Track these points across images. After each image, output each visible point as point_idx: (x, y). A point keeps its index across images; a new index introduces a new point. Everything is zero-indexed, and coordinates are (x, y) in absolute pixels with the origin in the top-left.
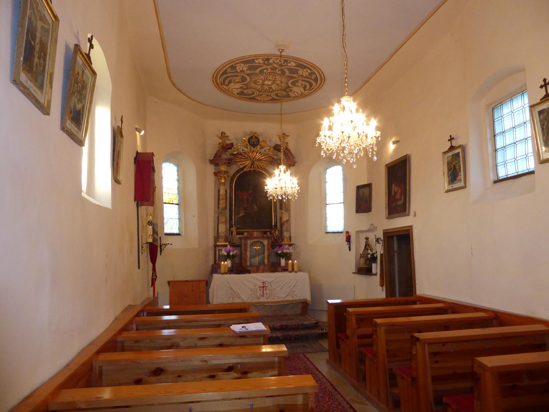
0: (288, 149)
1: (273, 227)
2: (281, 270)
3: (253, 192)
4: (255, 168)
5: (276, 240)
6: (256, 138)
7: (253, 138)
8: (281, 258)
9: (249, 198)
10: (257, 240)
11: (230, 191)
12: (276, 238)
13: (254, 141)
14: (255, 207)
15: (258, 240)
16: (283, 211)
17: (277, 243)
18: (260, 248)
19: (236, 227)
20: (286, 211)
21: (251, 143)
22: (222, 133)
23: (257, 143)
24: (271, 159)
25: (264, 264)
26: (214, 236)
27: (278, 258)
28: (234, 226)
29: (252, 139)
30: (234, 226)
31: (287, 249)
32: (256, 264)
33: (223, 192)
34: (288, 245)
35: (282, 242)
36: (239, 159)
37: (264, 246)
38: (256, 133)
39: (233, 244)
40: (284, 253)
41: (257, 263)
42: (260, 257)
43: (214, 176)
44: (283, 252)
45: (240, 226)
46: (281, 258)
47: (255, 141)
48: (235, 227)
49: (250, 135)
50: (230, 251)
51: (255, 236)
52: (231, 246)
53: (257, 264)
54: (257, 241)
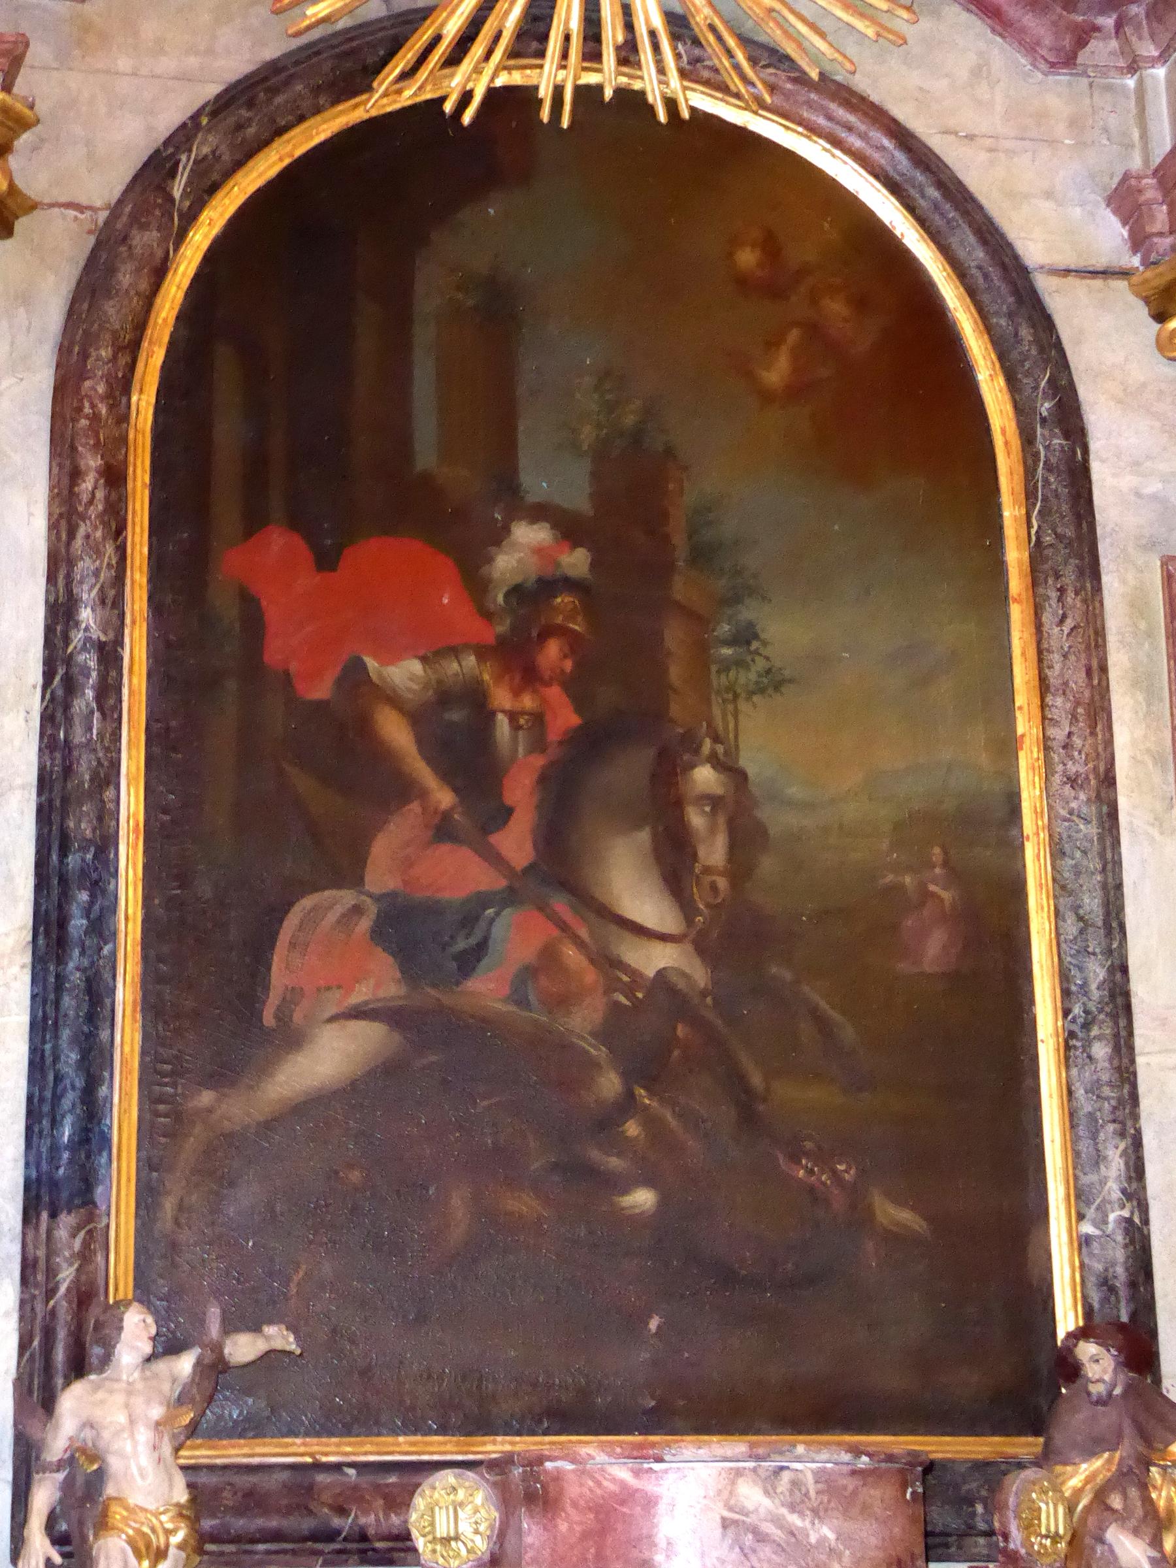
3: (577, 561)
9: (501, 698)
19: (185, 1364)
45: (279, 1337)
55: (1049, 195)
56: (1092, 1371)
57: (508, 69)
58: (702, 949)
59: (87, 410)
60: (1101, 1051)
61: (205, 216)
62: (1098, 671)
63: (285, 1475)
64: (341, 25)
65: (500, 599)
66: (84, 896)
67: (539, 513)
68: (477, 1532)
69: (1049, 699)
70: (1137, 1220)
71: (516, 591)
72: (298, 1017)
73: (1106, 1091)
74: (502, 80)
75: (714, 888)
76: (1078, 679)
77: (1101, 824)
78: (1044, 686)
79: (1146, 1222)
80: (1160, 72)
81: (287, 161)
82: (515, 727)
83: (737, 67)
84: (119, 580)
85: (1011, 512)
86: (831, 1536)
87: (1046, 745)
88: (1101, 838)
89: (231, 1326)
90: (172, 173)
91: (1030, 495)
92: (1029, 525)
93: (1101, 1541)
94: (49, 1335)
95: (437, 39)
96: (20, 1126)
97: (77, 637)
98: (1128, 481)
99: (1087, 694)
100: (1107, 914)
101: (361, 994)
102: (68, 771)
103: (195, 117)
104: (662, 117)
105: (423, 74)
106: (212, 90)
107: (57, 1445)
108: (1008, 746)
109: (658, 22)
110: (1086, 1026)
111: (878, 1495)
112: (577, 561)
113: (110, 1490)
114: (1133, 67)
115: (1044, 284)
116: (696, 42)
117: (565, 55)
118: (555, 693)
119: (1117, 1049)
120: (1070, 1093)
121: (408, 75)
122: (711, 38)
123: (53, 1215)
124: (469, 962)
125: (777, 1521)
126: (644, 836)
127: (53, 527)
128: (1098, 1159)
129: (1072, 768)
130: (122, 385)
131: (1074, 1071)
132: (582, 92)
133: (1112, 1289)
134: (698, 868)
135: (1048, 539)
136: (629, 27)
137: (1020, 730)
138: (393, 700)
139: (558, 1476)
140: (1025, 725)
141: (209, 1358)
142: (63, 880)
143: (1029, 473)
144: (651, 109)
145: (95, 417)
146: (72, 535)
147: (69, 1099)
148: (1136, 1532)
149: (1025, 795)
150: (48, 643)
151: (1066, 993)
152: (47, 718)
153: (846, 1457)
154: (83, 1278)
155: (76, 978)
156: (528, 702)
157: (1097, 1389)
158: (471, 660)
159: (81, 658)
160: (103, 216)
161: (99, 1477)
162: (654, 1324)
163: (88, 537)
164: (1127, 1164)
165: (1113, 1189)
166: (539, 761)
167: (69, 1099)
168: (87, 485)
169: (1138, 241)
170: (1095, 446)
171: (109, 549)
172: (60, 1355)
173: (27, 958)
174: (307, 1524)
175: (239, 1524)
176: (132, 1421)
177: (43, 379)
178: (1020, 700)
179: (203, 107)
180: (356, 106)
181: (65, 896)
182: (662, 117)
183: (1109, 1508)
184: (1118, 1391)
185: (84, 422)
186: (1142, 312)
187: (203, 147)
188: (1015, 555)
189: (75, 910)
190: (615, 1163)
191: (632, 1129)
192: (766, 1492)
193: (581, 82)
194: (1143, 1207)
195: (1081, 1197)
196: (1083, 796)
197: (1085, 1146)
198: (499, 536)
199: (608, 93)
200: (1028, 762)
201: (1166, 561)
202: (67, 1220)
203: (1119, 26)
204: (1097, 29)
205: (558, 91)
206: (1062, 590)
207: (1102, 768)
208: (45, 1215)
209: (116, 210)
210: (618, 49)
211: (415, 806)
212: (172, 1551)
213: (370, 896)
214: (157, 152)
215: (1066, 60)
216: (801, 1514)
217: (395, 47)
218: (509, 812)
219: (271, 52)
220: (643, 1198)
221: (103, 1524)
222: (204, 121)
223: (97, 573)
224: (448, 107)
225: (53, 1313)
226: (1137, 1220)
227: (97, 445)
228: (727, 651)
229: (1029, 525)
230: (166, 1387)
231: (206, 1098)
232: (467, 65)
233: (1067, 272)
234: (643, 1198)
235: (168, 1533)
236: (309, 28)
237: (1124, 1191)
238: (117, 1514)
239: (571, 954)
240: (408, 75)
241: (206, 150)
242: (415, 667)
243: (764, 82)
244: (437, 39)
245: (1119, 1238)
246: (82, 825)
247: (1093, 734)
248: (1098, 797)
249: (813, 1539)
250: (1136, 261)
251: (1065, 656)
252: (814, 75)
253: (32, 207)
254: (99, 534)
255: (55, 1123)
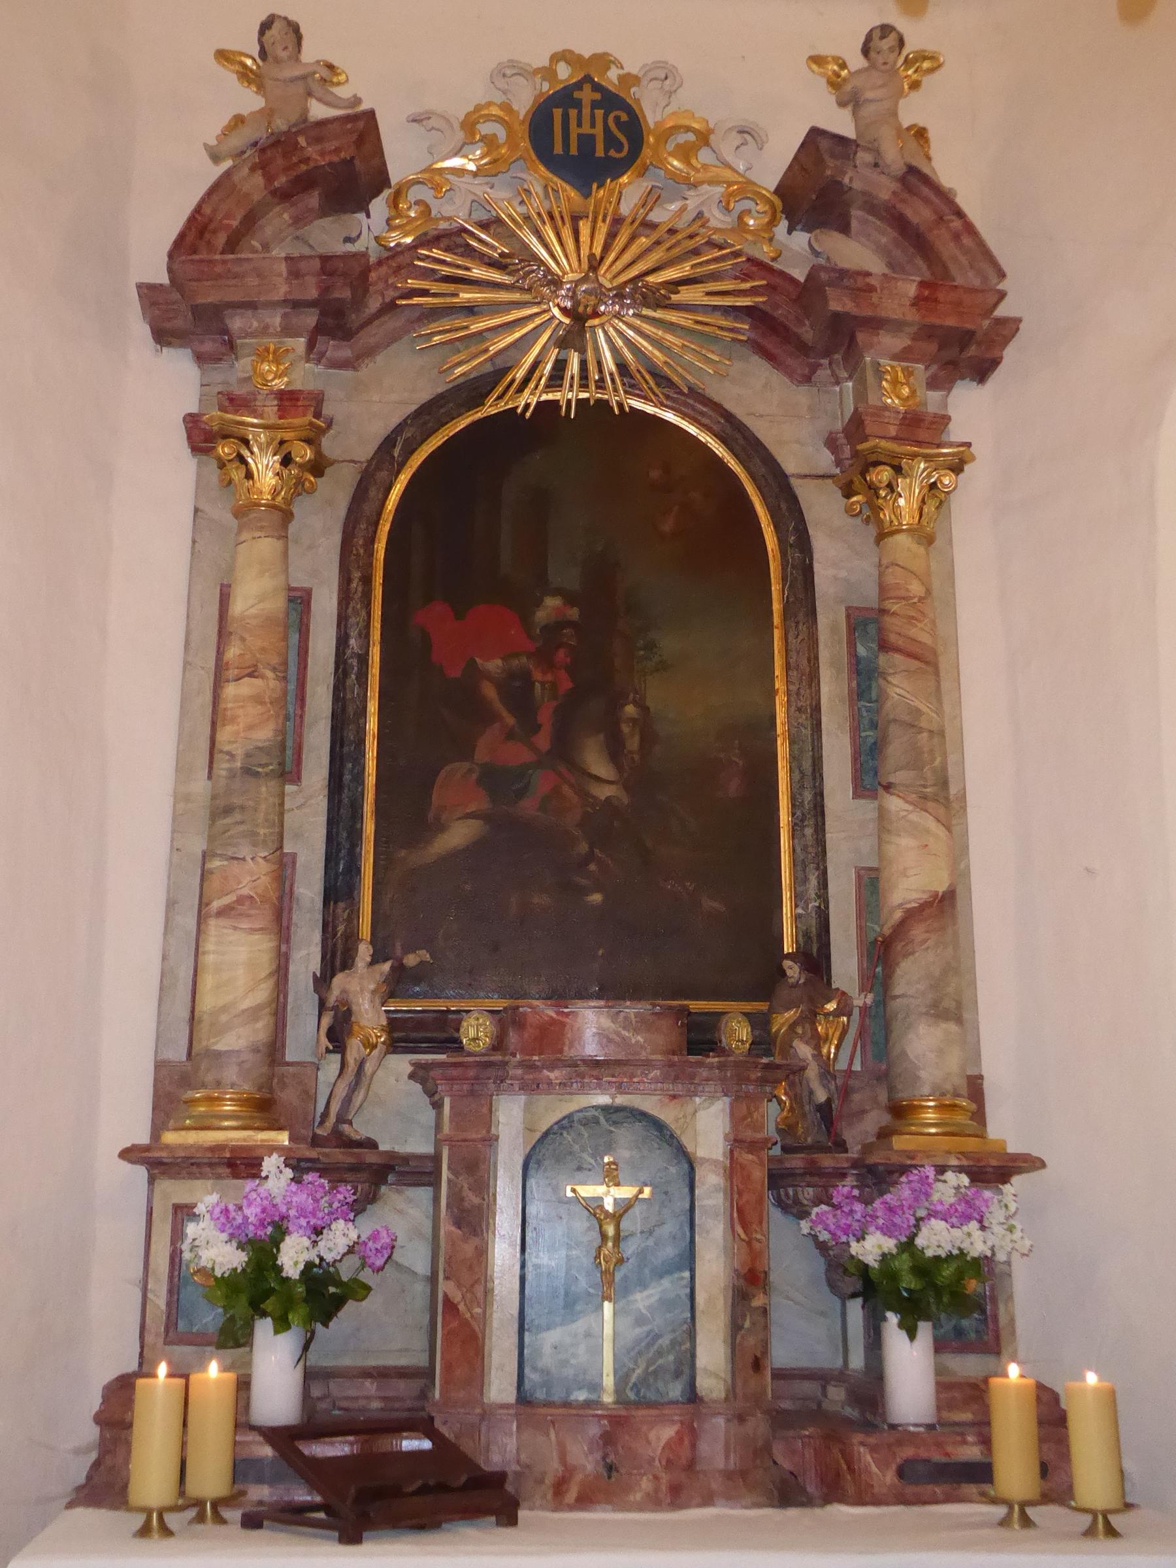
0: (927, 180)
1: (793, 970)
2: (890, 1477)
3: (574, 613)
4: (601, 384)
5: (825, 1111)
6: (610, 101)
7: (578, 104)
8: (893, 1319)
9: (537, 675)
10: (603, 1099)
11: (345, 597)
12: (821, 1096)
13: (586, 129)
14: (597, 763)
15: (620, 1100)
16: (894, 803)
17: (841, 1146)
18: (647, 1191)
19: (386, 967)
20: (922, 801)
21: (558, 149)
22: (265, 26)
23: (619, 148)
24: (753, 291)
25: (693, 1397)
26: (160, 1066)
27: (402, 306)
28: (364, 951)
29: (573, 113)
30: (364, 951)
31: (966, 1218)
32: (596, 1387)
33: (262, 598)
34: (960, 1169)
35: (885, 1134)
36: (435, 288)
37: (690, 1164)
38: (604, 61)
39: (351, 1143)
40: (926, 1268)
41: (609, 1381)
42: (643, 1300)
43: (188, 464)
44: (908, 1246)
45: (424, 955)
46: (893, 1319)
47: (599, 131)
48: (375, 961)
49: (548, 73)
50: (281, 1232)
51: (591, 1048)
52: (298, 1166)
53: (608, 1398)
54: (605, 1109)
55: (798, 442)
56: (789, 973)
57: (547, 393)
58: (626, 788)
59: (354, 552)
60: (809, 831)
61: (410, 462)
62: (814, 660)
63: (435, 1015)
64: (472, 376)
65: (538, 630)
66: (350, 765)
67: (557, 592)
68: (486, 1036)
69: (790, 673)
70: (822, 907)
71: (545, 628)
72: (444, 817)
73: (810, 849)
74: (544, 397)
75: (633, 758)
76: (804, 663)
77: (812, 729)
78: (788, 667)
79: (827, 907)
80: (850, 384)
81: (446, 438)
82: (543, 688)
83: (651, 389)
84: (368, 626)
85: (775, 588)
86: (642, 1040)
87: (788, 693)
88: (812, 735)
89: (410, 949)
90: (394, 446)
91: (784, 579)
92: (784, 594)
93: (792, 1047)
94: (334, 955)
95: (513, 381)
96: (323, 864)
97: (349, 652)
98: (831, 572)
99: (808, 670)
100: (814, 770)
101: (472, 808)
102: (344, 709)
103: (405, 420)
104: (616, 411)
105: (507, 397)
106: (414, 407)
107: (332, 1001)
108: (773, 693)
109: (613, 368)
110: (802, 821)
111: (665, 1023)
112: (574, 613)
113: (353, 1019)
114: (838, 383)
115: (794, 482)
116: (632, 377)
117: (571, 386)
118: (563, 674)
119: (816, 831)
120: (794, 850)
121: (500, 397)
122: (638, 376)
123: (336, 903)
124: (521, 794)
125: (618, 1034)
126: (601, 737)
127: (340, 603)
128: (805, 880)
129: (800, 704)
130: (371, 540)
131: (796, 841)
132: (580, 402)
133: (810, 938)
134: (625, 751)
135: (791, 600)
136: (601, 371)
137: (777, 687)
138: (487, 676)
139: (525, 1014)
140: (779, 685)
141: (396, 964)
142: (341, 758)
143: (784, 569)
144: (612, 408)
145: (358, 555)
146: (347, 608)
147: (343, 853)
148: (807, 1043)
149: (778, 717)
150: (337, 655)
151: (793, 806)
152: (336, 689)
153: (650, 1007)
154: (348, 930)
155: (346, 801)
156: (549, 677)
157: (791, 981)
158: (524, 660)
159: (350, 661)
160: (365, 465)
161: (349, 1012)
162: (600, 952)
163: (354, 607)
164: (818, 882)
165: (812, 893)
166: (555, 703)
167: (343, 853)
168: (354, 585)
169: (838, 463)
170: (816, 556)
171: (364, 613)
172: (338, 963)
173: (326, 792)
174: (445, 1035)
175: (414, 1035)
176: (362, 990)
177: (337, 538)
178: (777, 673)
179: (409, 416)
180: (477, 412)
181: (342, 766)
182: (616, 411)
183: (796, 1033)
184: (802, 981)
185: (353, 557)
186: (839, 493)
187: (407, 433)
188: (777, 607)
189: (346, 772)
190: (584, 882)
191: (592, 867)
192: (613, 1022)
193: (580, 397)
194: (826, 902)
195: (798, 898)
196: (804, 717)
197: (800, 874)
198: (539, 603)
199: (592, 402)
200: (780, 701)
201: (848, 609)
202: (341, 905)
203: (830, 364)
204: (821, 365)
205: (569, 402)
206: (797, 623)
207: (814, 703)
208: (332, 903)
209: (370, 462)
210: (596, 382)
211: (497, 725)
212: (379, 1045)
213: (477, 764)
214: (389, 436)
215: (807, 379)
216: (628, 1031)
217: (496, 384)
218: (540, 726)
219: (440, 390)
220: (596, 898)
221: (350, 1033)
222: (409, 422)
223: (358, 624)
224: (519, 411)
225: (335, 945)
226: (822, 907)
227: (358, 567)
228: (642, 653)
229: (784, 594)
230: (378, 977)
231: (403, 853)
232: (527, 392)
233: (806, 476)
234: (596, 898)
235: (377, 1037)
236: (456, 378)
237: (816, 894)
238: (356, 1028)
239: (566, 790)
240: (500, 397)
241: (409, 435)
242: (499, 662)
243: (663, 393)
244: (513, 381)
245: (814, 915)
246: (350, 735)
247: (810, 686)
248: (811, 716)
249: (633, 1041)
250: (838, 471)
251: (798, 653)
252: (686, 390)
253: (332, 463)
254: (359, 606)
255: (337, 864)
